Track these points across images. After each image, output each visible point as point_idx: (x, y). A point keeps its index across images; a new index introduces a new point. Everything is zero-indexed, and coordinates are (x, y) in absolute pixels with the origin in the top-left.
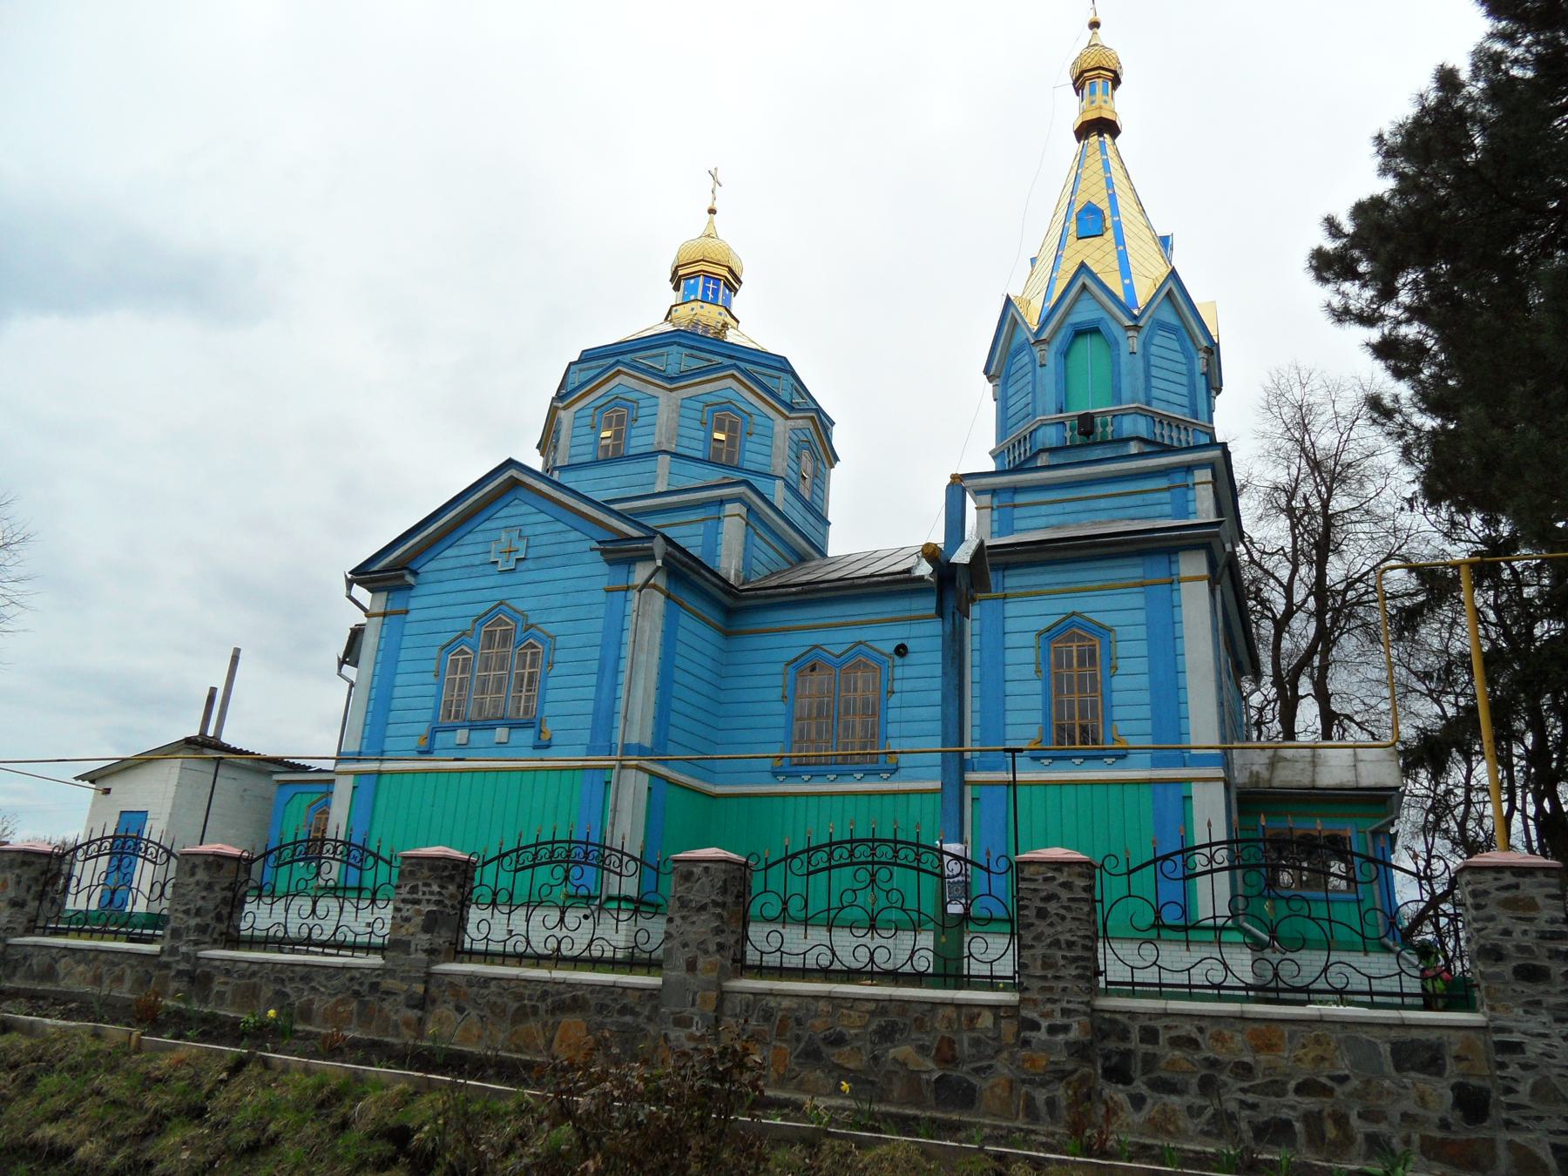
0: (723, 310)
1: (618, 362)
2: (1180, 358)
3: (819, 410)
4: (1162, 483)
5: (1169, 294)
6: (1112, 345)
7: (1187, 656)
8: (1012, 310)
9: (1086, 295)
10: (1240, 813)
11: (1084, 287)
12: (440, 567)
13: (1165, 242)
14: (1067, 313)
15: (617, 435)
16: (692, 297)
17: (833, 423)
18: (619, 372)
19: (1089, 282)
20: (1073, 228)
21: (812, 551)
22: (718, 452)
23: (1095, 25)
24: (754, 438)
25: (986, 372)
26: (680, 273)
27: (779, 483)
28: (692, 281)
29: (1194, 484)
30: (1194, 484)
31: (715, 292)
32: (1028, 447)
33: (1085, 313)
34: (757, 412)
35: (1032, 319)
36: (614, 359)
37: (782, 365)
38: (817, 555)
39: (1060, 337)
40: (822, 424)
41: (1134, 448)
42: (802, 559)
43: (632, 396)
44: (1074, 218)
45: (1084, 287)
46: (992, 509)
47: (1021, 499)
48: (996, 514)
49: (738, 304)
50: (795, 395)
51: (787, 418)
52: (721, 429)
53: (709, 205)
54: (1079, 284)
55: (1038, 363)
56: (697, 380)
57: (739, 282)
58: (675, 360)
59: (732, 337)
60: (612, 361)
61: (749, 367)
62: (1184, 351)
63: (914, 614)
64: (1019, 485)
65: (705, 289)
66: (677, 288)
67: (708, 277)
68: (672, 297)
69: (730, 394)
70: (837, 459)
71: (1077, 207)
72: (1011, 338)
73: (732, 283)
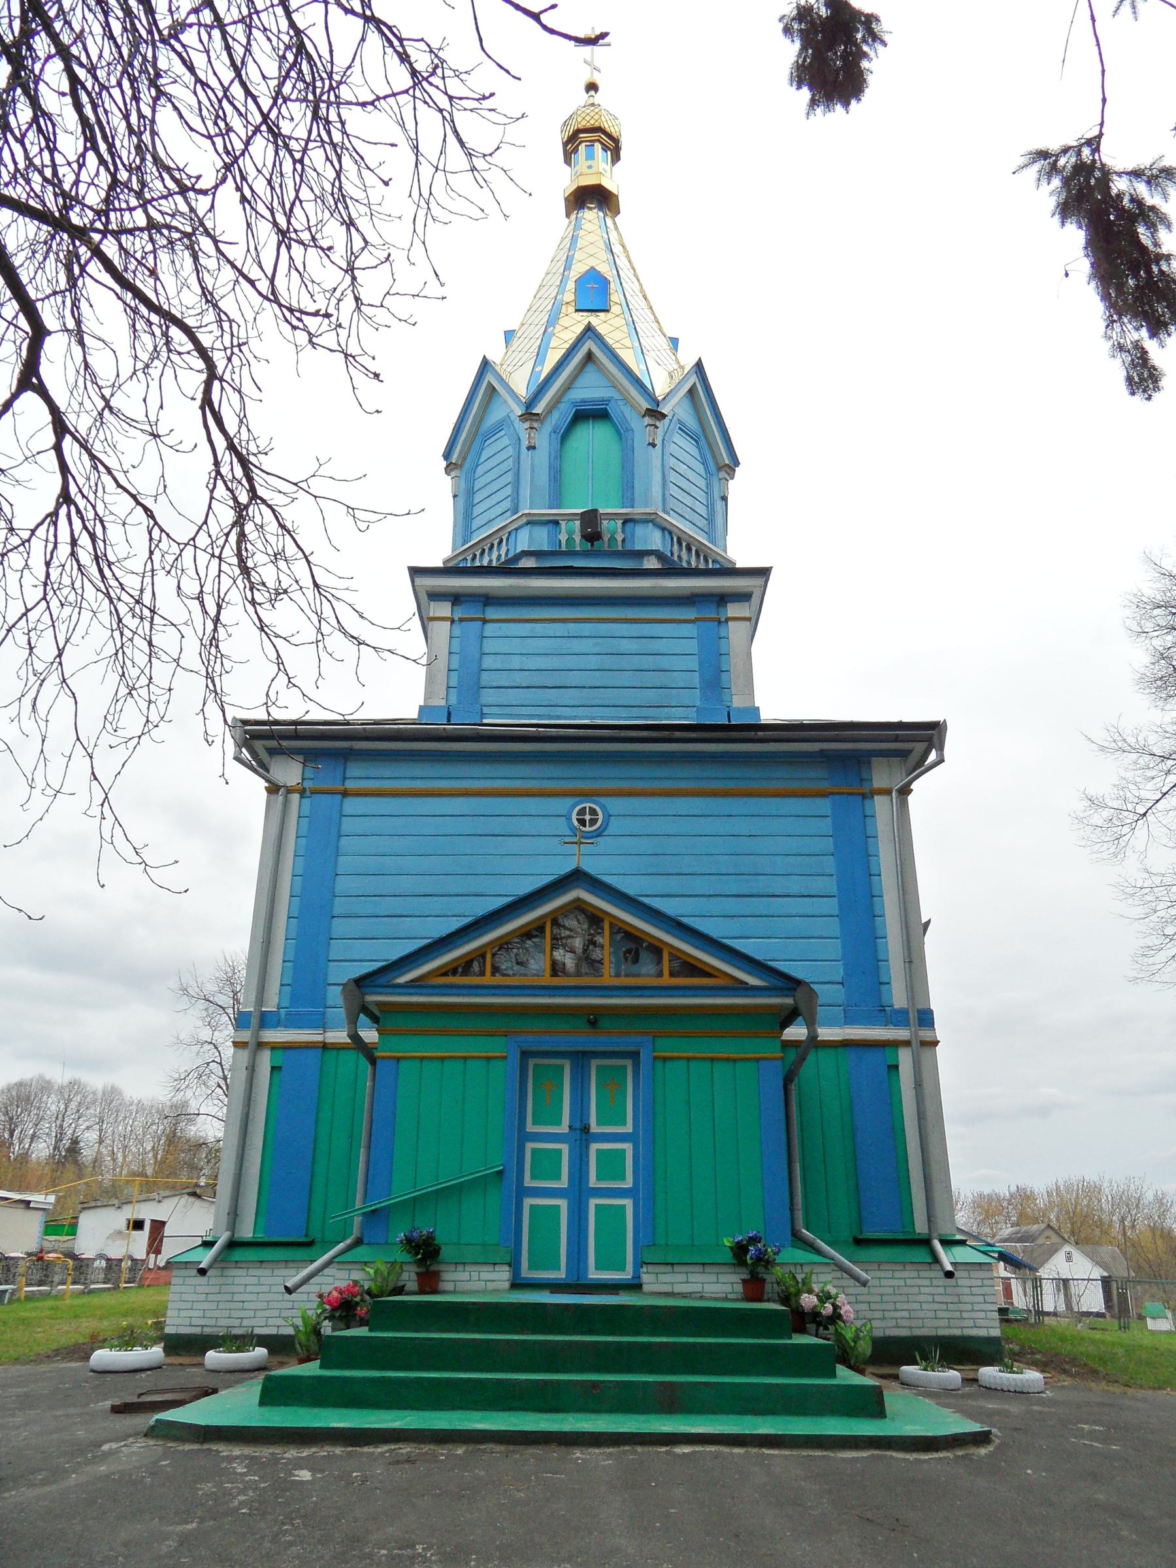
4: (689, 613)
5: (692, 392)
6: (622, 434)
7: (885, 898)
8: (489, 377)
9: (590, 368)
10: (686, 962)
11: (590, 356)
12: (623, 712)
13: (674, 342)
14: (568, 387)
19: (596, 351)
20: (569, 296)
23: (592, 87)
25: (447, 455)
29: (728, 620)
30: (728, 620)
32: (503, 552)
33: (590, 389)
35: (521, 383)
39: (556, 415)
41: (652, 563)
44: (571, 285)
45: (590, 356)
46: (453, 621)
47: (492, 613)
48: (457, 631)
55: (525, 444)
63: (359, 963)
64: (492, 593)
71: (575, 273)
72: (481, 421)
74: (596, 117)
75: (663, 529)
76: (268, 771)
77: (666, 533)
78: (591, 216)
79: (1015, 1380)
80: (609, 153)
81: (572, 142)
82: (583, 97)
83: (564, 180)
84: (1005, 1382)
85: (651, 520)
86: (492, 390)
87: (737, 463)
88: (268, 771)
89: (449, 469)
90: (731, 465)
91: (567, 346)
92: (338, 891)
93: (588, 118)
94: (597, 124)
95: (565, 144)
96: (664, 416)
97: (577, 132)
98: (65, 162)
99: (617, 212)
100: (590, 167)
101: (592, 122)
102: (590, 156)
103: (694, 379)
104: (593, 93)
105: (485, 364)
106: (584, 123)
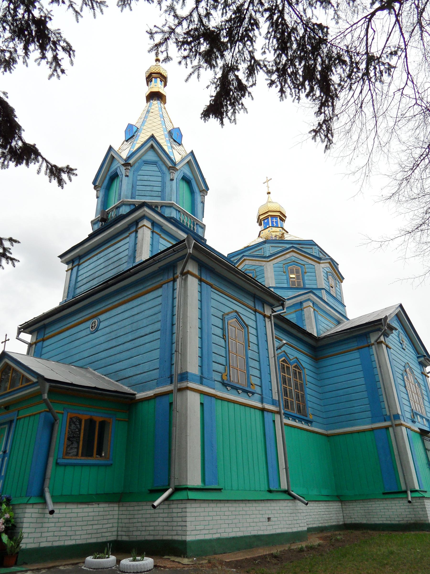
0: (281, 229)
1: (244, 256)
2: (159, 174)
3: (331, 259)
5: (189, 163)
8: (112, 153)
15: (298, 277)
16: (268, 226)
17: (338, 265)
18: (245, 260)
21: (341, 317)
22: (293, 283)
24: (308, 274)
25: (94, 183)
26: (261, 218)
27: (323, 292)
28: (266, 221)
31: (277, 222)
34: (305, 263)
36: (242, 255)
37: (312, 243)
38: (345, 320)
40: (333, 264)
42: (339, 322)
43: (253, 268)
49: (286, 225)
50: (320, 254)
51: (319, 263)
52: (292, 273)
53: (267, 191)
54: (149, 145)
56: (273, 258)
57: (285, 217)
58: (268, 250)
59: (287, 237)
60: (239, 257)
61: (249, 252)
62: (161, 171)
65: (272, 222)
66: (260, 225)
67: (272, 216)
68: (259, 228)
69: (293, 259)
70: (343, 279)
73: (282, 217)
74: (159, 69)
75: (177, 210)
76: (307, 416)
77: (177, 212)
78: (156, 103)
79: (137, 565)
80: (163, 82)
81: (149, 78)
82: (154, 63)
83: (146, 90)
84: (142, 567)
85: (171, 206)
86: (113, 158)
87: (208, 189)
88: (307, 416)
89: (95, 188)
90: (205, 190)
91: (142, 143)
92: (26, 346)
93: (155, 69)
94: (158, 72)
95: (147, 78)
96: (177, 170)
97: (151, 74)
98: (154, 234)
99: (165, 103)
100: (155, 85)
101: (157, 70)
102: (156, 82)
103: (190, 158)
104: (158, 62)
105: (111, 148)
106: (154, 71)
